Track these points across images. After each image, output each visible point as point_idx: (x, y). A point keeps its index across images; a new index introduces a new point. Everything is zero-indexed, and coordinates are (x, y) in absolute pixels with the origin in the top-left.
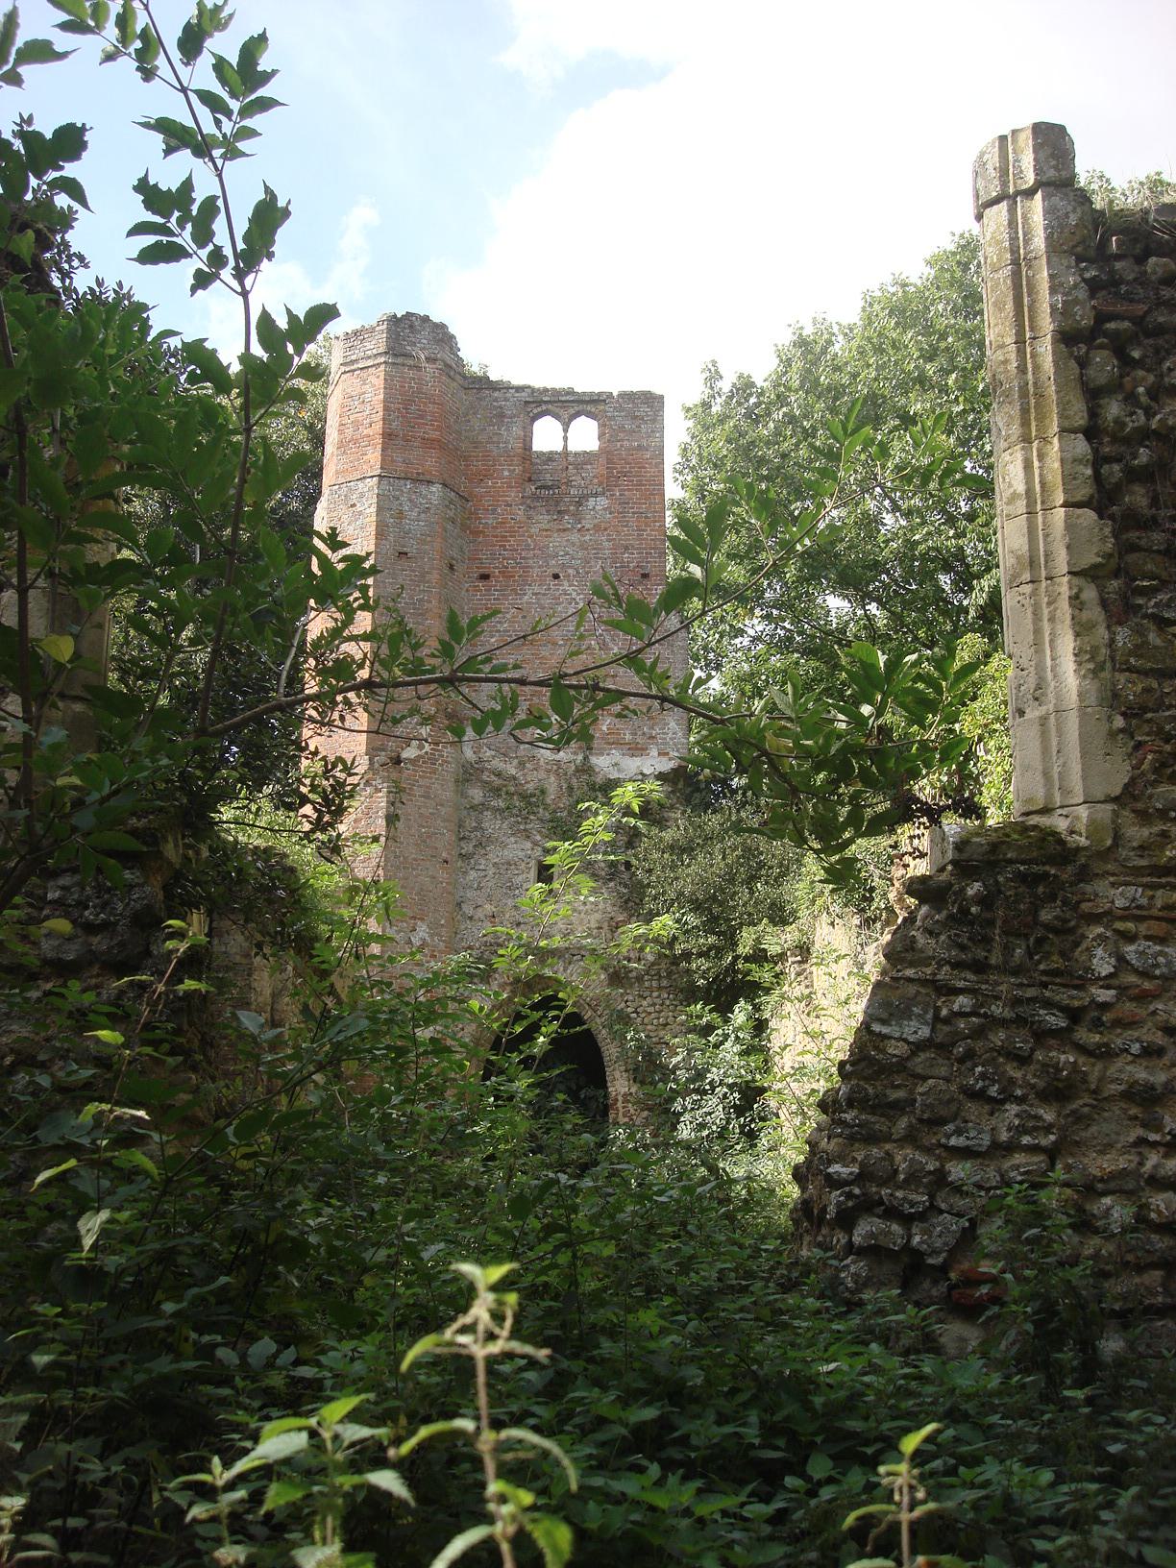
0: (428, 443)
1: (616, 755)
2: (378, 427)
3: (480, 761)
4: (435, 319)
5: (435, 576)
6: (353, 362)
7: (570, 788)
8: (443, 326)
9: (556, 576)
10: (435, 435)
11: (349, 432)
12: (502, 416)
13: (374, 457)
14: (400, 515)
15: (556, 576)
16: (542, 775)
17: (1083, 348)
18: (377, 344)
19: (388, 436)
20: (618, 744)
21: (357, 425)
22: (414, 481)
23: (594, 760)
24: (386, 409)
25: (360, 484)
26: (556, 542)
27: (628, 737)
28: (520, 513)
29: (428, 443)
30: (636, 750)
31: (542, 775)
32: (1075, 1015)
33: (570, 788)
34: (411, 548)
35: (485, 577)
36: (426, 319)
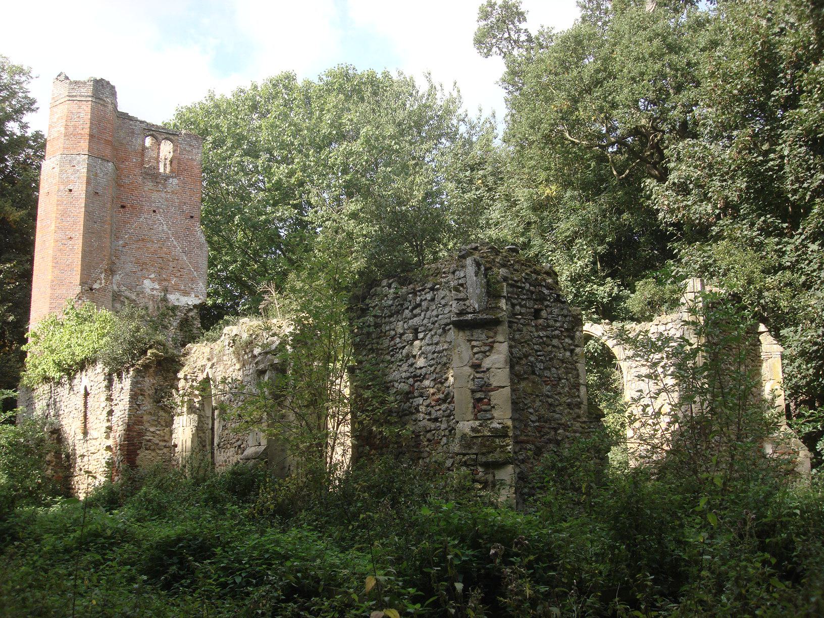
0: (107, 142)
1: (177, 295)
2: (87, 131)
3: (120, 291)
4: (112, 83)
5: (109, 205)
6: (73, 96)
7: (158, 307)
8: (113, 87)
9: (154, 211)
10: (110, 139)
11: (71, 130)
12: (133, 133)
13: (84, 145)
14: (96, 175)
15: (154, 211)
16: (147, 300)
17: (519, 433)
18: (88, 90)
19: (91, 136)
20: (179, 290)
21: (75, 127)
22: (102, 159)
23: (168, 296)
24: (91, 123)
25: (78, 157)
26: (155, 195)
27: (183, 288)
28: (140, 179)
29: (107, 142)
30: (186, 293)
31: (147, 300)
32: (29, 534)
33: (158, 307)
34: (100, 192)
35: (123, 207)
36: (108, 83)
